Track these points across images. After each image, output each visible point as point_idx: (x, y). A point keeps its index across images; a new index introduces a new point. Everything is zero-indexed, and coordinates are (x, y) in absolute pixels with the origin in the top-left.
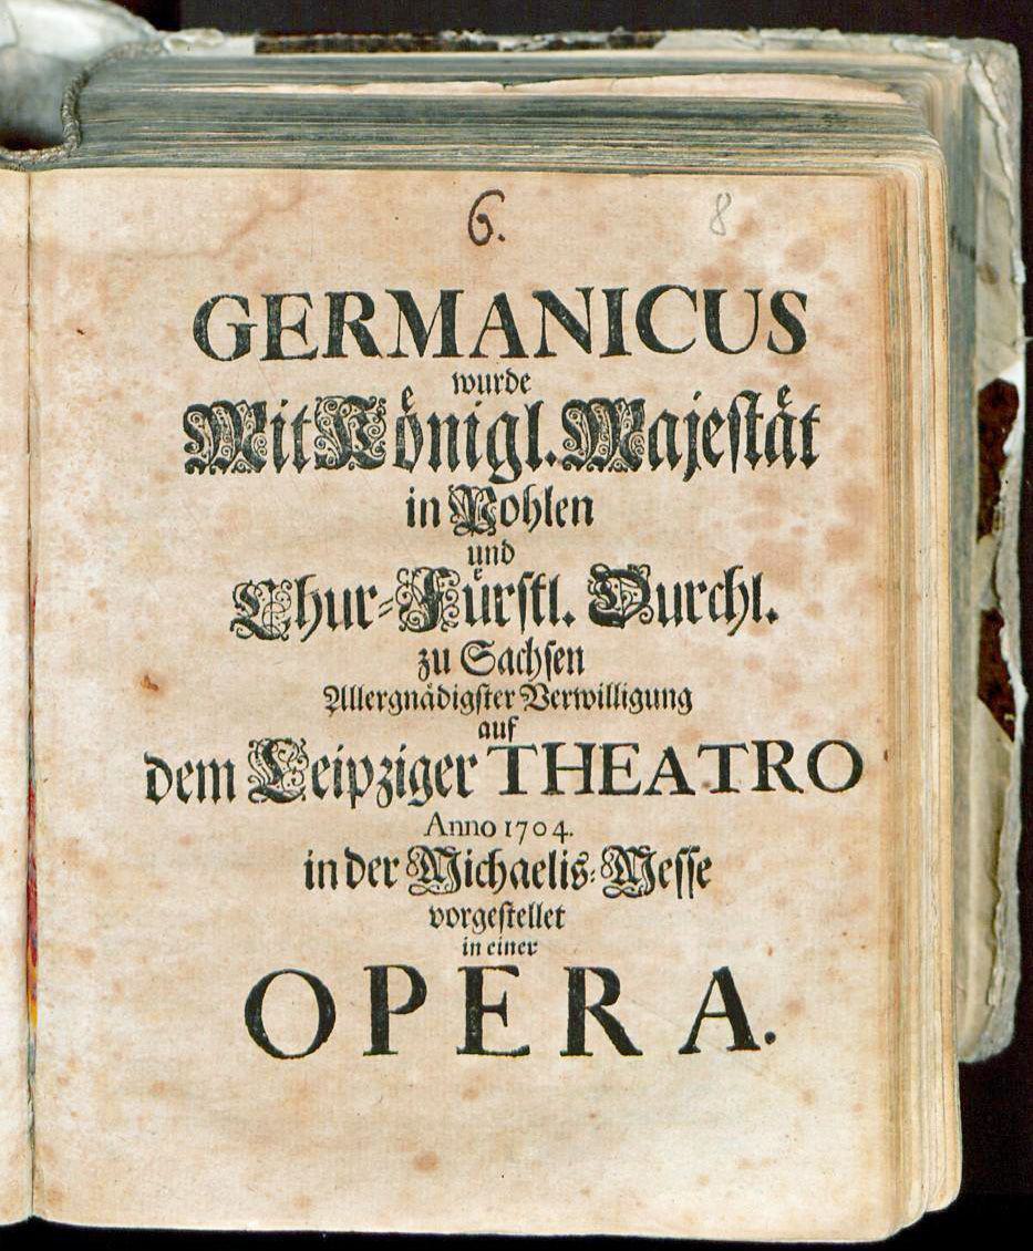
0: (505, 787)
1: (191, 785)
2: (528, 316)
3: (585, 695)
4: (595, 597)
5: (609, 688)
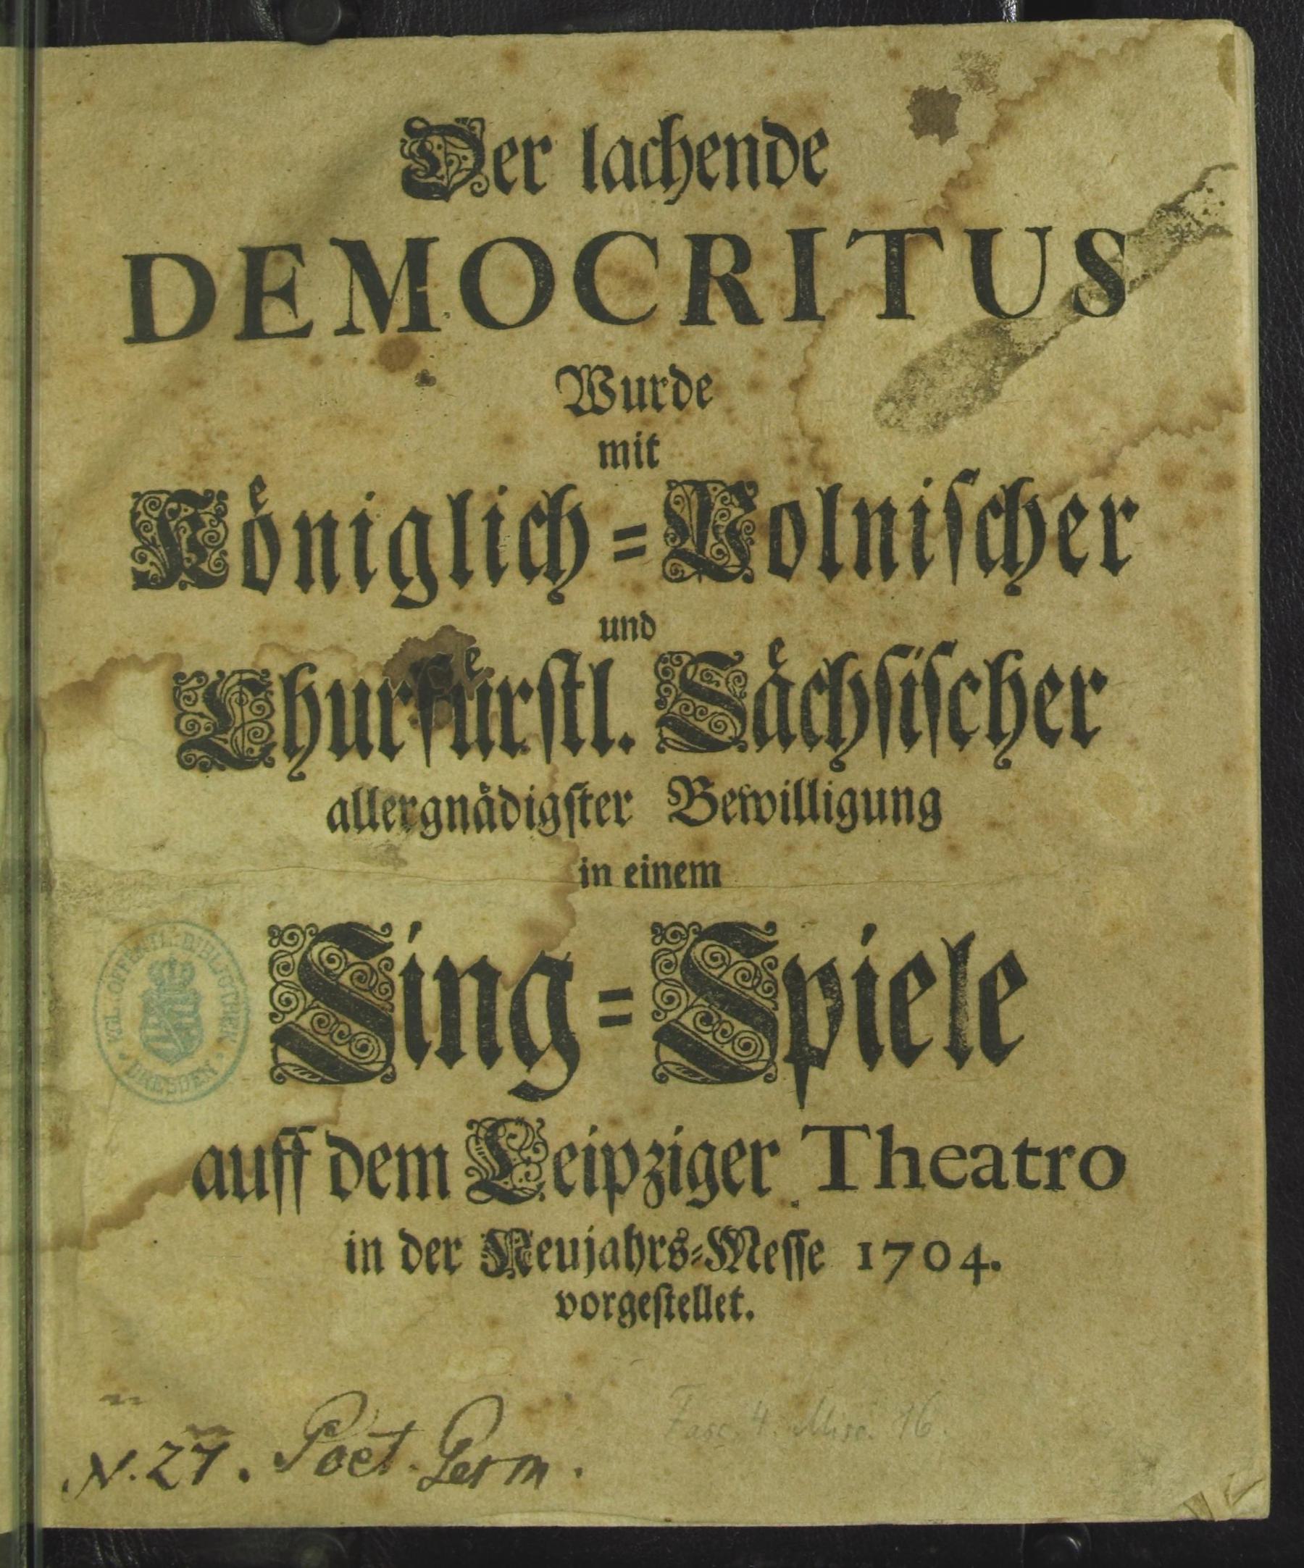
0: (827, 1179)
1: (388, 1175)
4: (410, 161)
5: (798, 786)
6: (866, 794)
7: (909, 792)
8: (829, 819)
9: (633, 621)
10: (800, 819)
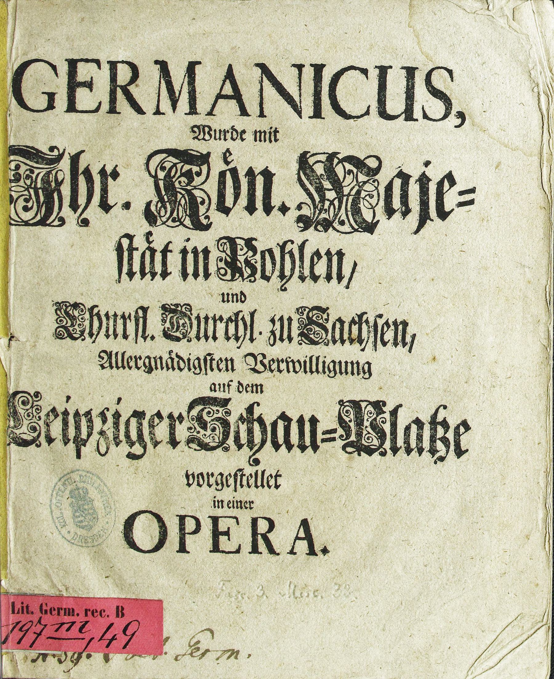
2: (249, 81)
3: (294, 363)
5: (311, 358)
6: (340, 362)
7: (161, 358)
8: (324, 372)
9: (237, 295)
10: (312, 372)
